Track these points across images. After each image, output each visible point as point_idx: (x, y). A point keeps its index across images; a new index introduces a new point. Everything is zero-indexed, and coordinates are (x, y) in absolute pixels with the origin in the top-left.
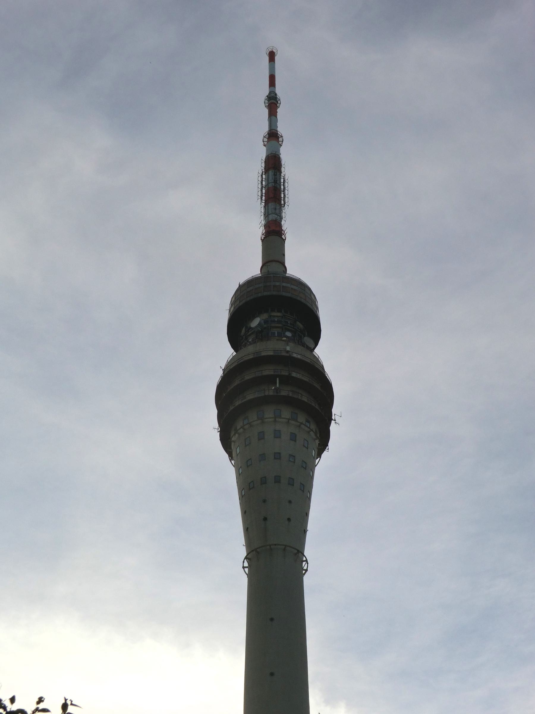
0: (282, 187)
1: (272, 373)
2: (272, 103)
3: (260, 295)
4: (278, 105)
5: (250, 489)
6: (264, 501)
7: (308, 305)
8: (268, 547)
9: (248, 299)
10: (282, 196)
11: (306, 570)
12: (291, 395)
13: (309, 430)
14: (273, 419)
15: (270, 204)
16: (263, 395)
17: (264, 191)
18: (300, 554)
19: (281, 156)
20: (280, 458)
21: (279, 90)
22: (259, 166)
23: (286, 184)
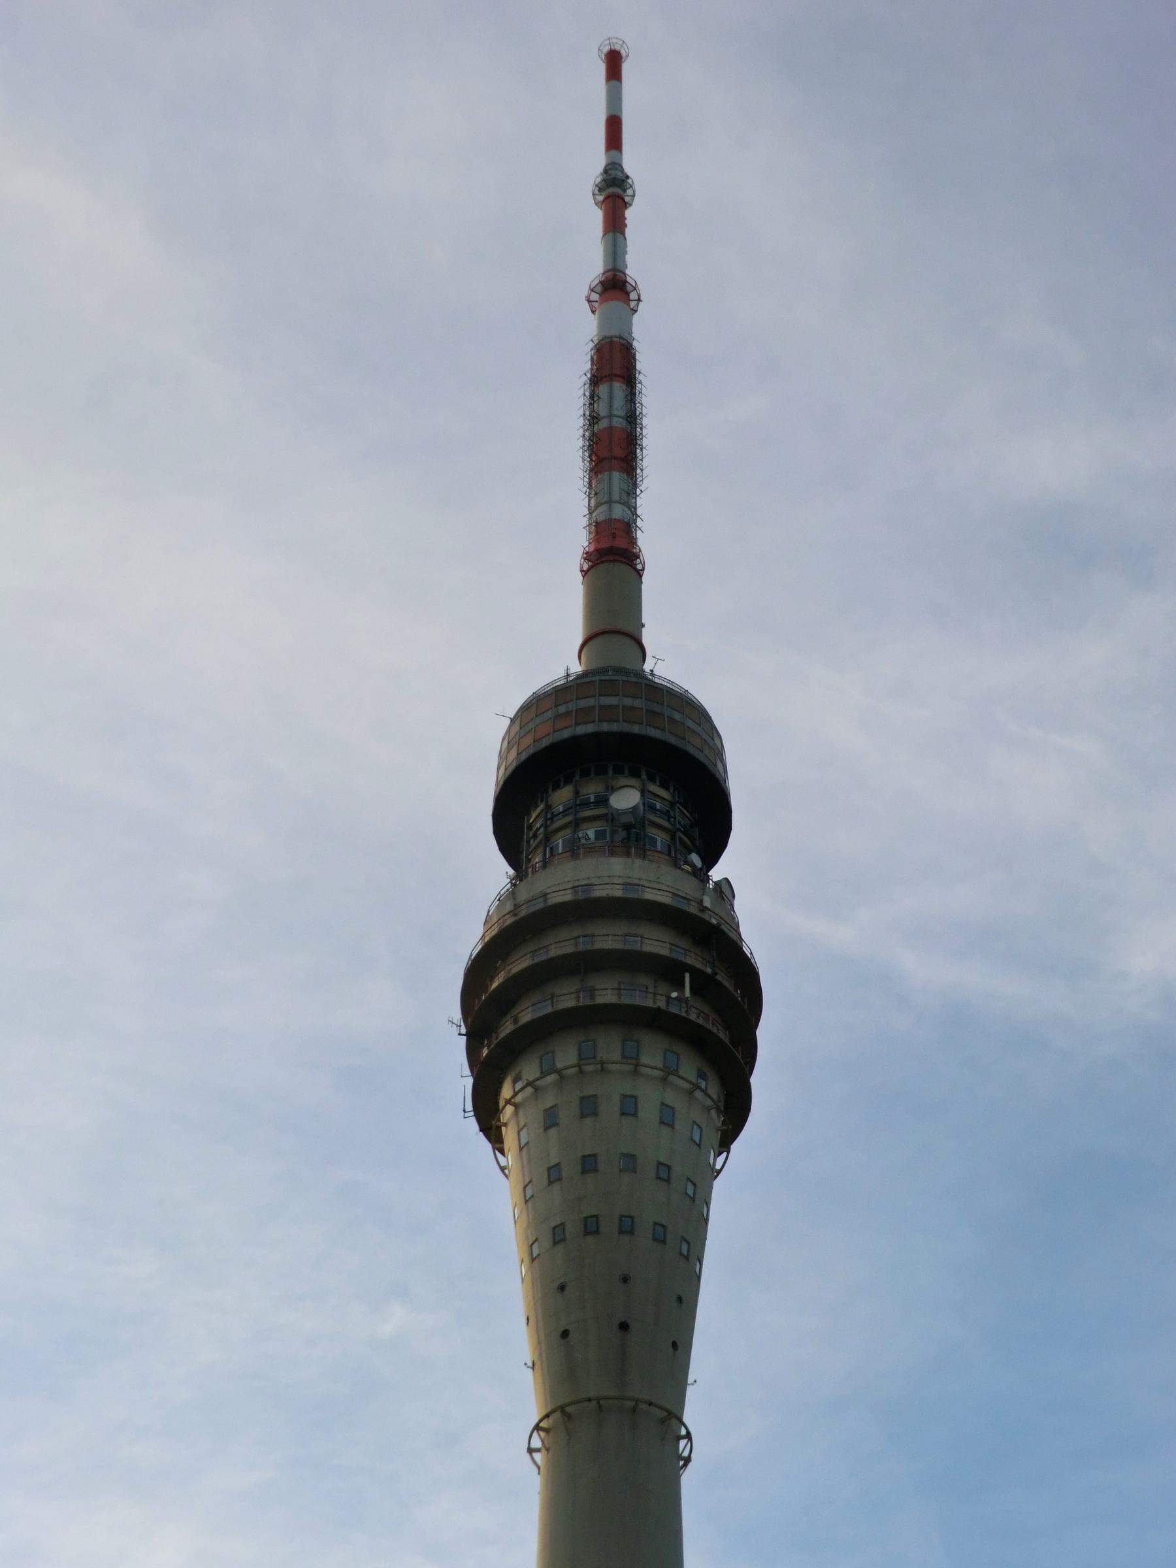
2: (614, 192)
7: (692, 750)
8: (594, 1403)
11: (688, 1460)
19: (635, 344)
21: (630, 162)
22: (581, 365)
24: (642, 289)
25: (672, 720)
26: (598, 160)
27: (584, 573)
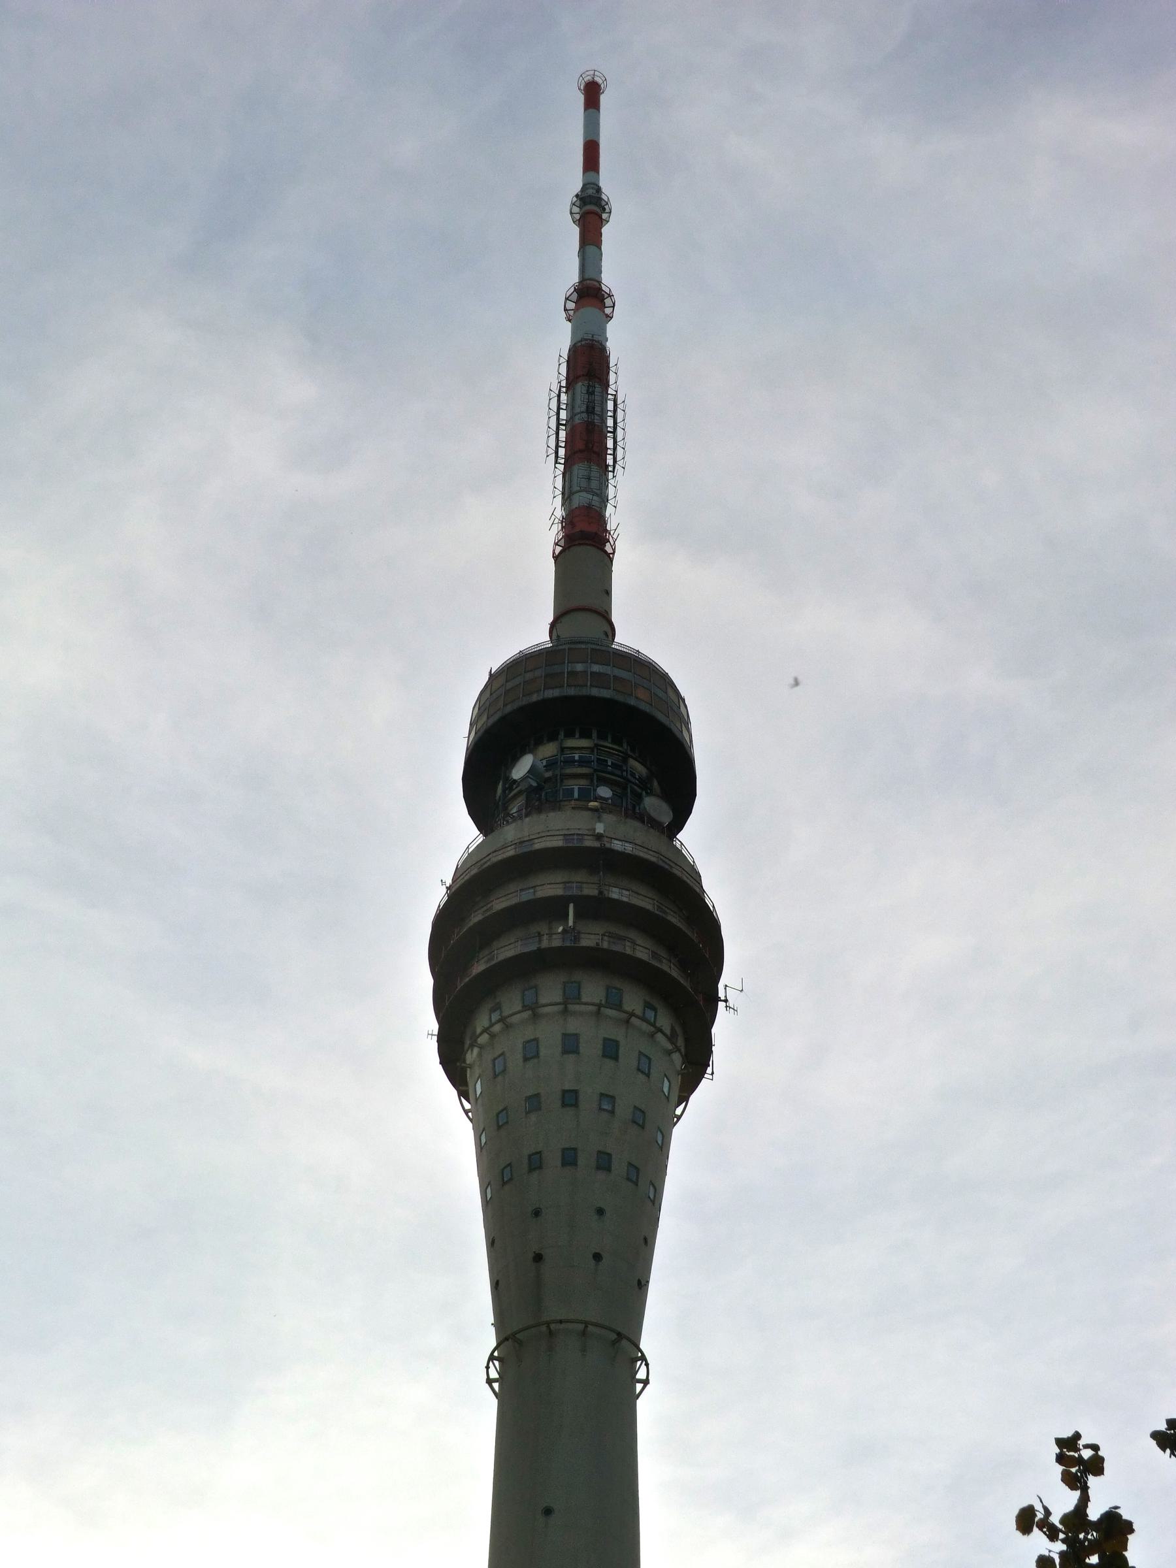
0: (610, 422)
1: (558, 891)
2: (591, 212)
3: (535, 698)
4: (604, 216)
5: (504, 1183)
6: (537, 1213)
9: (509, 709)
10: (610, 444)
11: (646, 1382)
12: (605, 945)
13: (652, 1029)
14: (561, 1007)
15: (576, 468)
16: (533, 947)
17: (563, 434)
18: (624, 1343)
20: (576, 1105)
23: (620, 414)
24: (616, 298)
25: (572, 674)
26: (575, 182)
27: (556, 558)
